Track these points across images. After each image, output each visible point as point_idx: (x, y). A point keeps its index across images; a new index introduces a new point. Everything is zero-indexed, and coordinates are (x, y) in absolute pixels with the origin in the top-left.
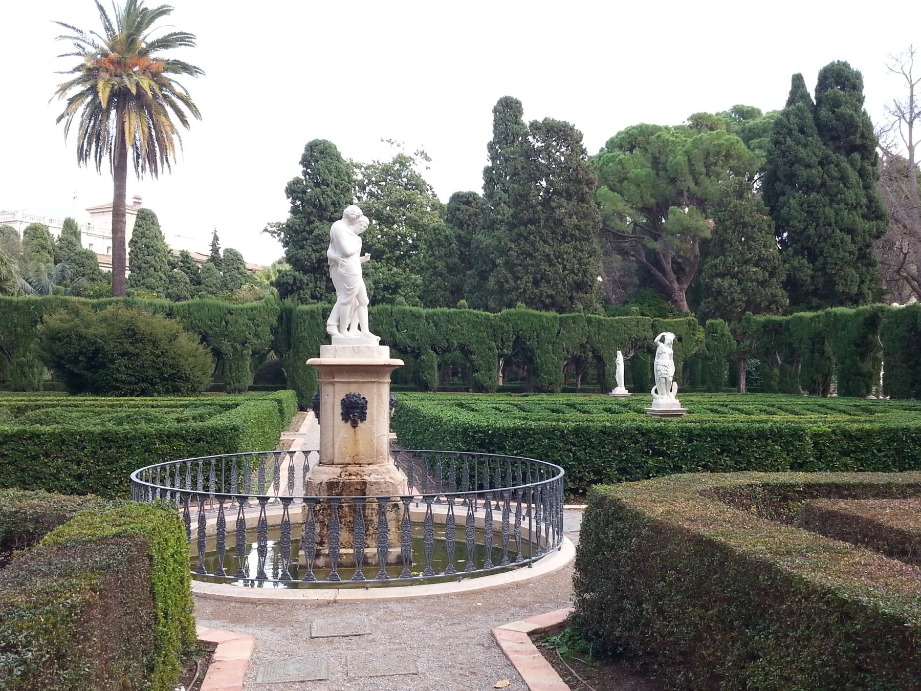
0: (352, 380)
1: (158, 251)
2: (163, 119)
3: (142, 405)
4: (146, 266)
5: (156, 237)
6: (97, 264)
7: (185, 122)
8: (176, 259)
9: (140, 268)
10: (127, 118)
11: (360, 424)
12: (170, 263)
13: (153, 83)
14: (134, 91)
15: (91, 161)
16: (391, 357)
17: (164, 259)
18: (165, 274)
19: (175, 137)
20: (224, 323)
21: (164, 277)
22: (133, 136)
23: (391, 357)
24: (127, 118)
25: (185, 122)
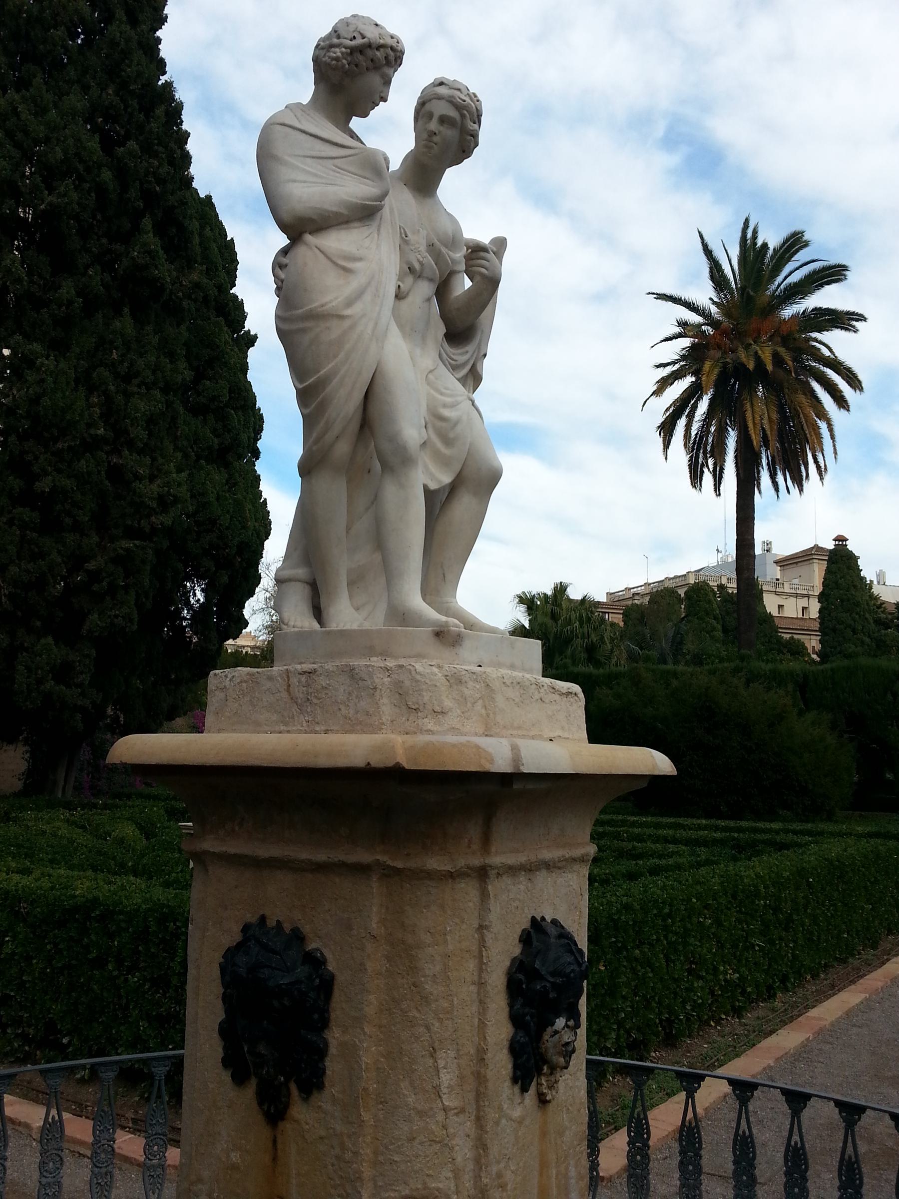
0: (264, 851)
1: (858, 604)
2: (802, 398)
3: (650, 836)
4: (842, 627)
5: (855, 586)
6: (775, 629)
7: (841, 402)
8: (890, 617)
9: (834, 630)
10: (748, 406)
11: (299, 1110)
12: (878, 622)
13: (781, 350)
14: (751, 366)
15: (708, 479)
16: (597, 735)
17: (867, 615)
18: (869, 636)
19: (823, 426)
20: (889, 697)
21: (867, 640)
22: (759, 427)
23: (597, 735)
24: (748, 406)
25: (841, 402)
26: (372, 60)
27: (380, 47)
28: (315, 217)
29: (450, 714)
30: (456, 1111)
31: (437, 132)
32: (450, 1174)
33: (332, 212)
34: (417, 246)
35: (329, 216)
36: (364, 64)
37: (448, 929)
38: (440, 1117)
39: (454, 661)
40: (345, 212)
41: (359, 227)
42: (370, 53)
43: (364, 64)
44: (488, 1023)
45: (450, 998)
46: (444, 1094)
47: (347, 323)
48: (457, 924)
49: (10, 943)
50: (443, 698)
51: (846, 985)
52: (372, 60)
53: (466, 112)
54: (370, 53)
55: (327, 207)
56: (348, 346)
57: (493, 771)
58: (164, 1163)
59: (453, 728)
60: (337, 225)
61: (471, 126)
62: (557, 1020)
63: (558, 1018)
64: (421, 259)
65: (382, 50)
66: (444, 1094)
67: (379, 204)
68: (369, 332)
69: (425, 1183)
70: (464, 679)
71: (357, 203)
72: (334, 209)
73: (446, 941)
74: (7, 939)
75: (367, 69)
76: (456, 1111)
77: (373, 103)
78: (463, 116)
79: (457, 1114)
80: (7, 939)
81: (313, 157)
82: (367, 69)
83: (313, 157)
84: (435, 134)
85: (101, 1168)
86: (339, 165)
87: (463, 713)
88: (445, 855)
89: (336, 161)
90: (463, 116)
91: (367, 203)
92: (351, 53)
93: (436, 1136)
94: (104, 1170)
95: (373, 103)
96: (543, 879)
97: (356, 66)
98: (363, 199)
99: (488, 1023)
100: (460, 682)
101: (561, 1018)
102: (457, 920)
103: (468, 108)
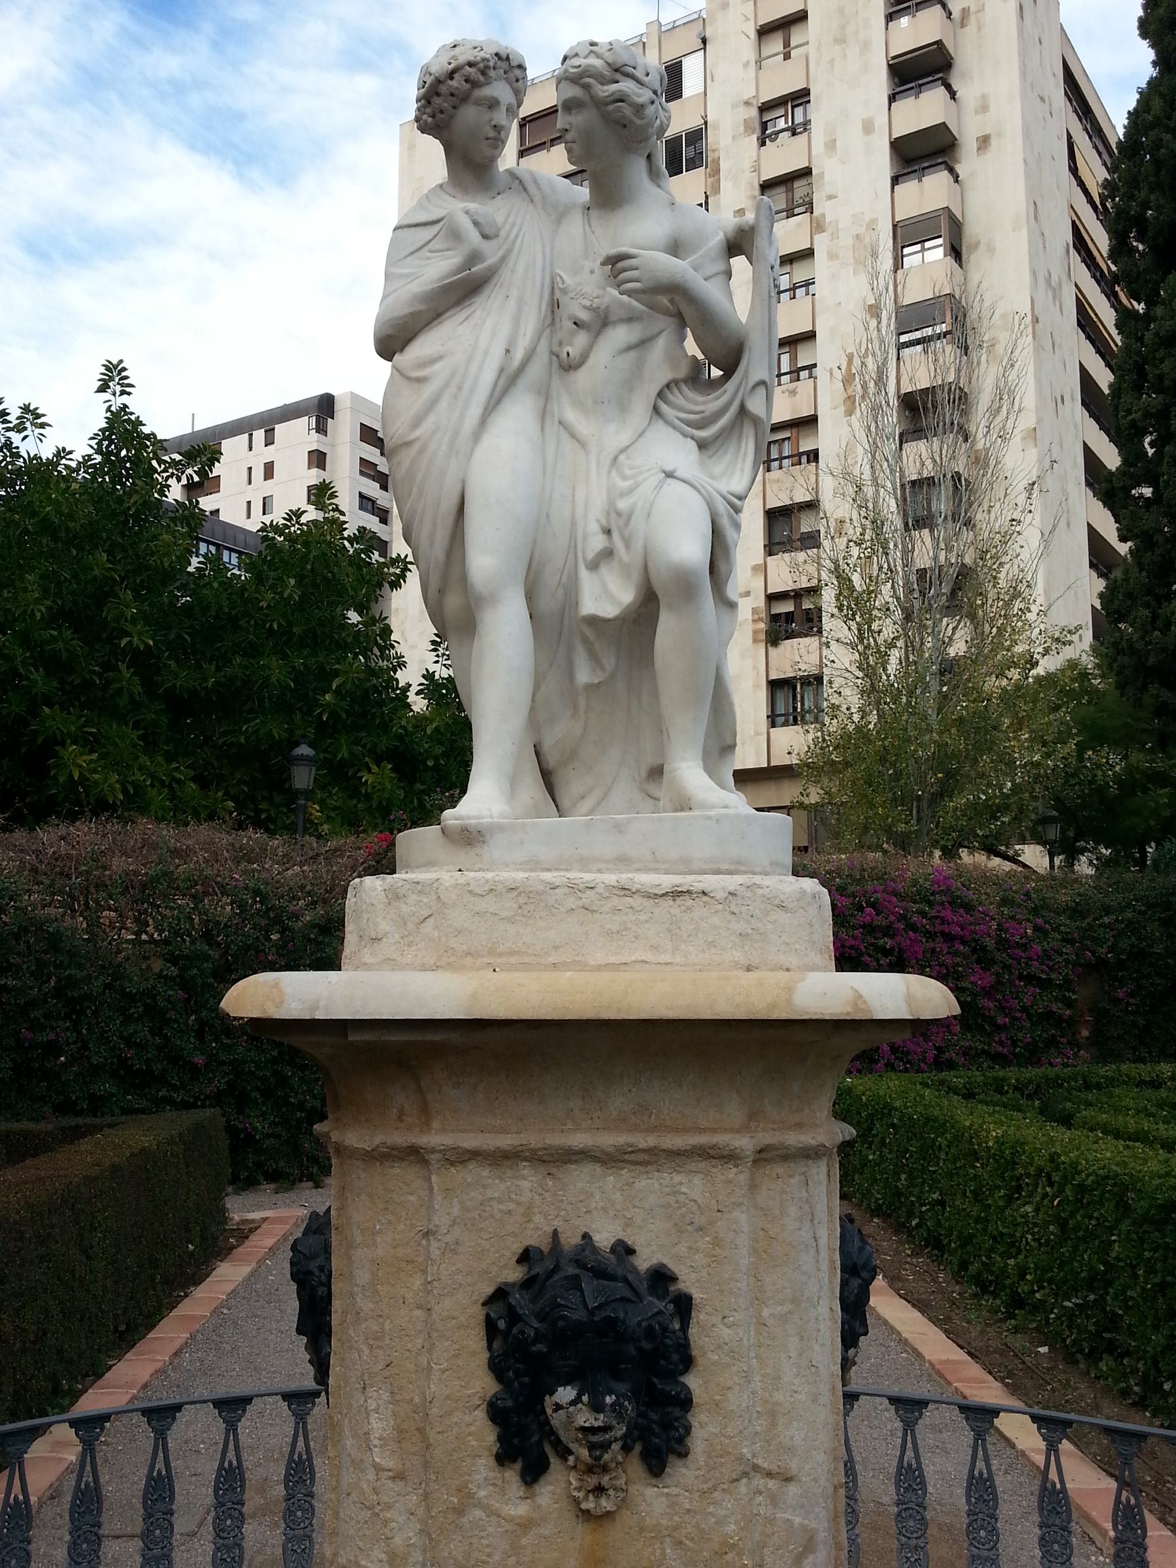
26: (452, 95)
27: (451, 75)
28: (391, 332)
29: (384, 940)
30: (391, 1474)
31: (567, 127)
32: (383, 1556)
33: (405, 316)
34: (579, 288)
35: (405, 322)
36: (446, 105)
37: (378, 1227)
38: (371, 1475)
39: (473, 865)
40: (422, 307)
41: (454, 314)
42: (443, 89)
43: (446, 105)
44: (434, 1366)
45: (380, 1320)
46: (375, 1446)
47: (416, 447)
48: (390, 1222)
49: (1117, 1244)
50: (379, 920)
51: (1094, 1449)
52: (452, 95)
53: (587, 80)
54: (443, 89)
55: (401, 313)
56: (419, 476)
57: (278, 1017)
58: (994, 1557)
59: (389, 959)
60: (434, 319)
61: (604, 92)
62: (560, 1389)
63: (565, 1385)
64: (588, 304)
65: (456, 76)
66: (375, 1446)
67: (468, 274)
68: (444, 448)
69: (356, 1557)
70: (402, 892)
71: (432, 289)
72: (407, 311)
73: (375, 1243)
74: (1113, 1238)
75: (454, 107)
76: (391, 1474)
77: (487, 139)
78: (587, 87)
79: (393, 1478)
80: (1113, 1238)
81: (412, 253)
82: (454, 107)
83: (412, 253)
84: (566, 130)
85: (909, 1538)
86: (433, 249)
87: (402, 937)
88: (369, 1128)
89: (431, 246)
90: (587, 87)
91: (446, 282)
92: (429, 102)
93: (365, 1499)
94: (913, 1542)
95: (487, 139)
96: (581, 1177)
97: (442, 112)
98: (440, 280)
99: (434, 1366)
100: (397, 897)
101: (569, 1388)
102: (391, 1217)
103: (588, 74)
